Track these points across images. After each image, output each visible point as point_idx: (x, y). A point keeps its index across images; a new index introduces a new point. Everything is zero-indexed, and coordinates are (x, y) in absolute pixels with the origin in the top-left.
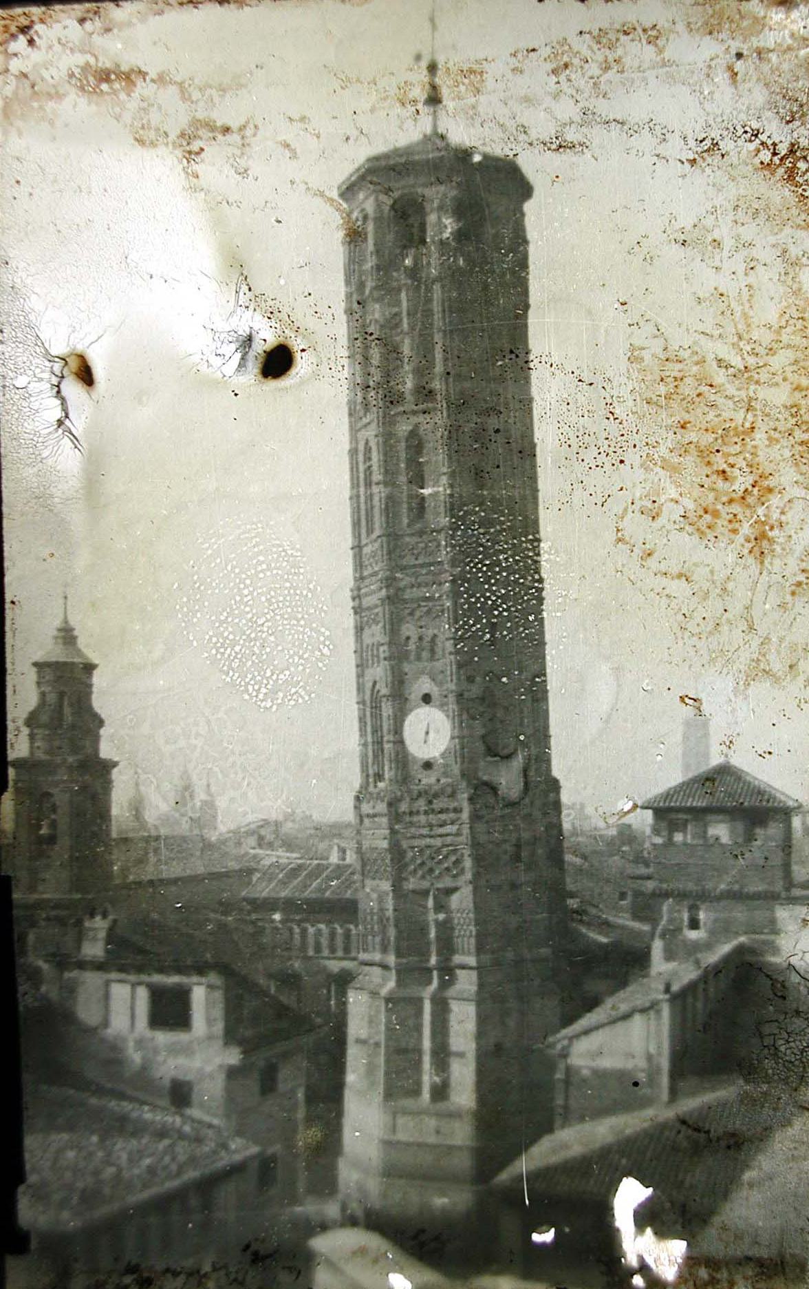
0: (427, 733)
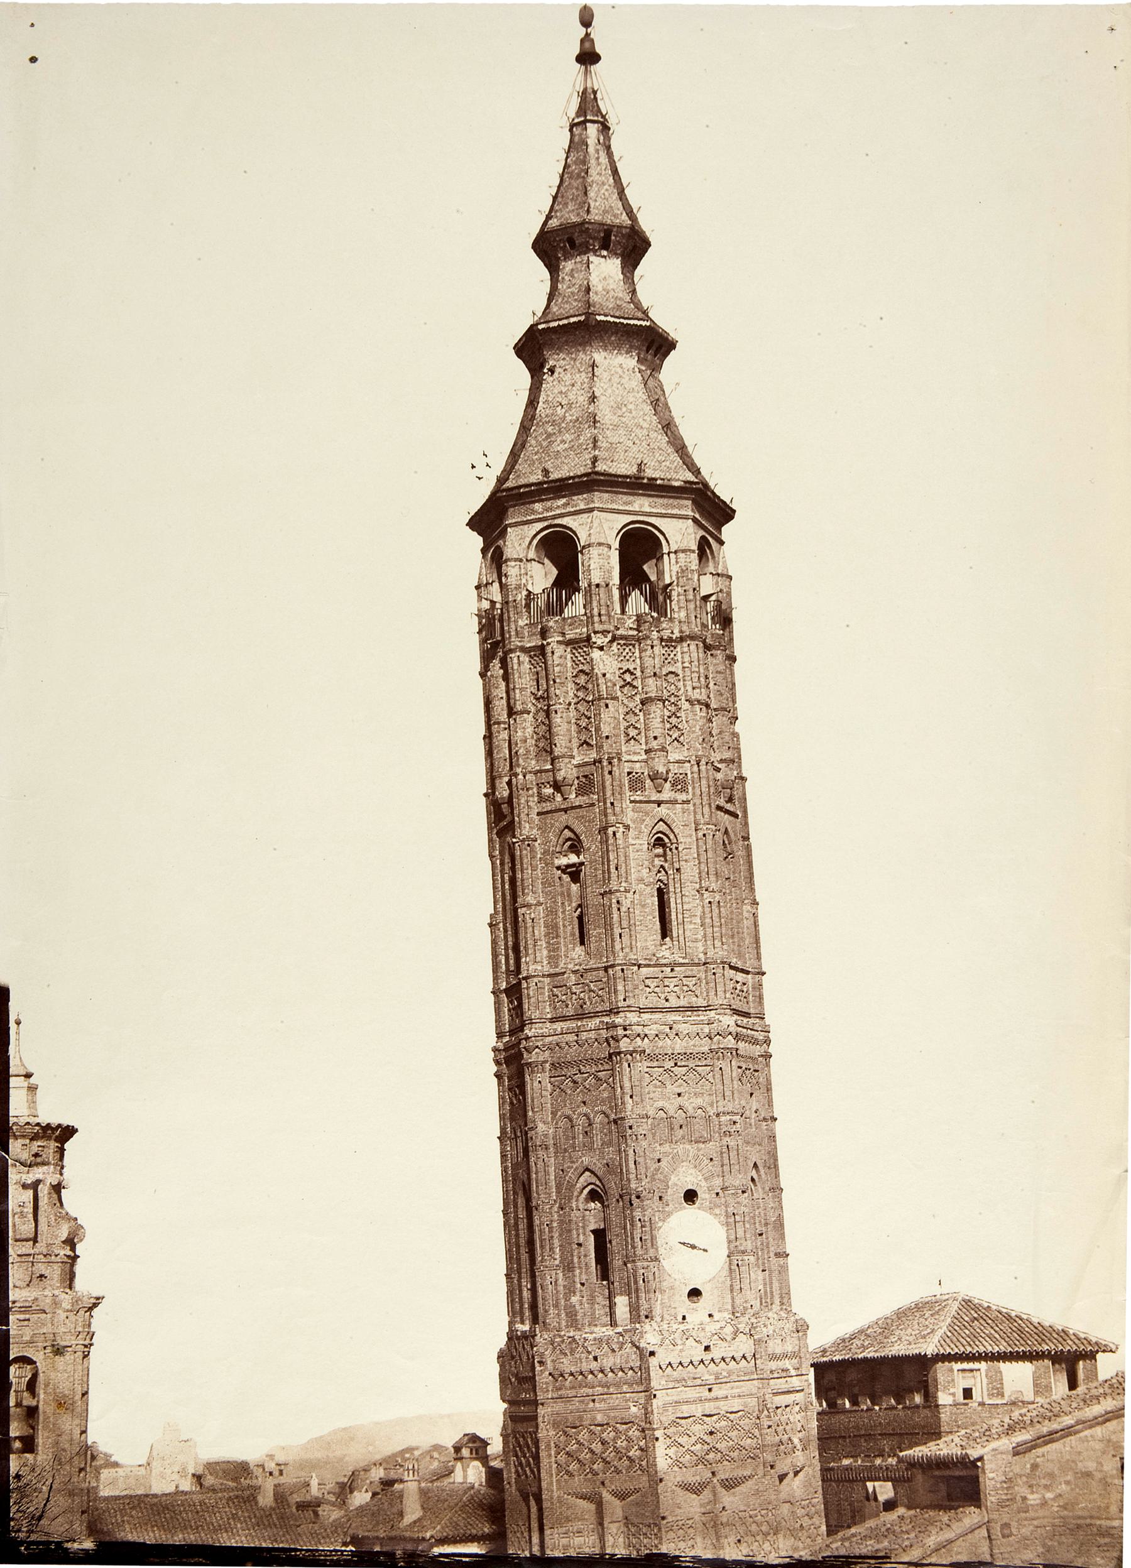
0: (693, 1247)
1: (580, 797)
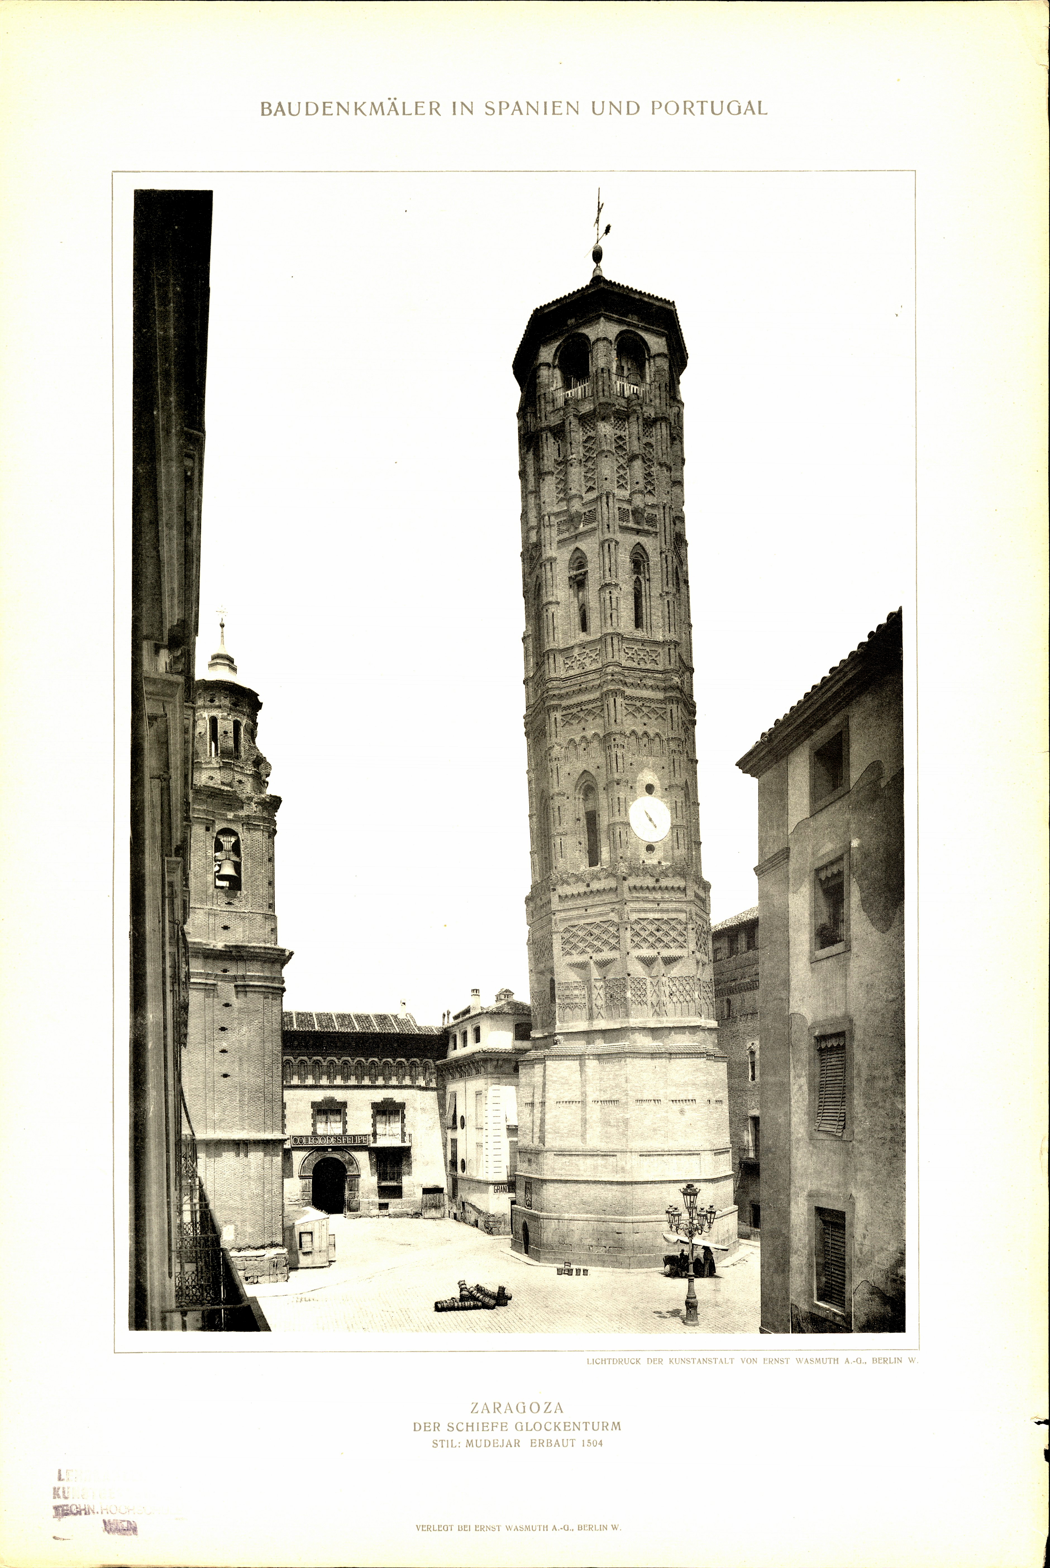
0: (650, 820)
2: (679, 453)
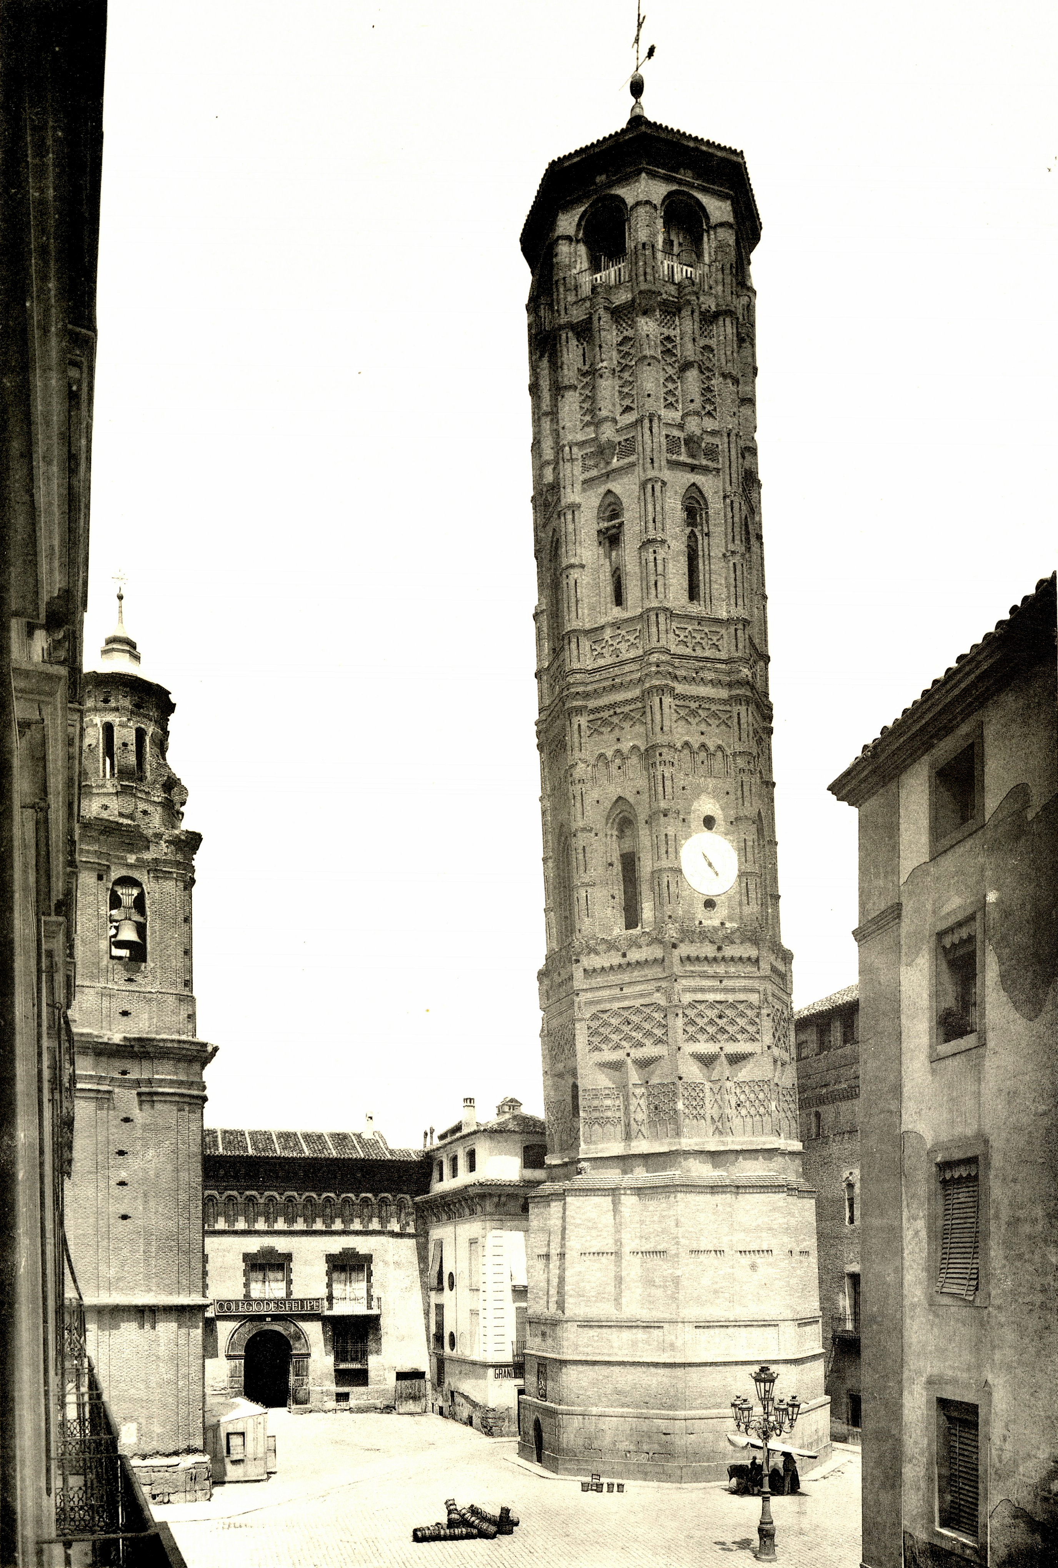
0: (710, 865)
1: (621, 460)
2: (750, 360)
